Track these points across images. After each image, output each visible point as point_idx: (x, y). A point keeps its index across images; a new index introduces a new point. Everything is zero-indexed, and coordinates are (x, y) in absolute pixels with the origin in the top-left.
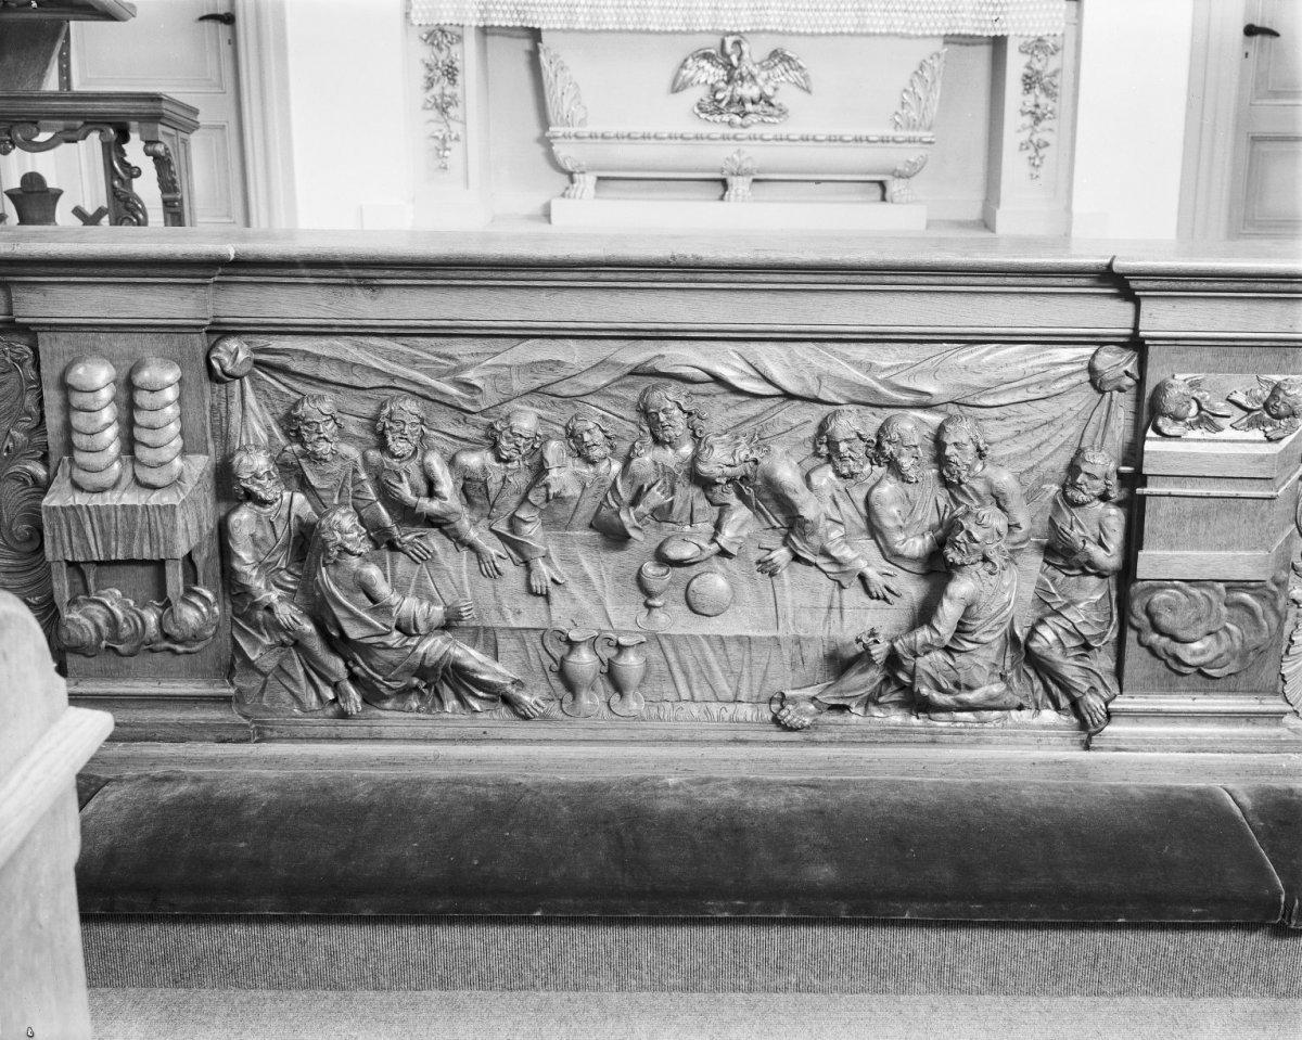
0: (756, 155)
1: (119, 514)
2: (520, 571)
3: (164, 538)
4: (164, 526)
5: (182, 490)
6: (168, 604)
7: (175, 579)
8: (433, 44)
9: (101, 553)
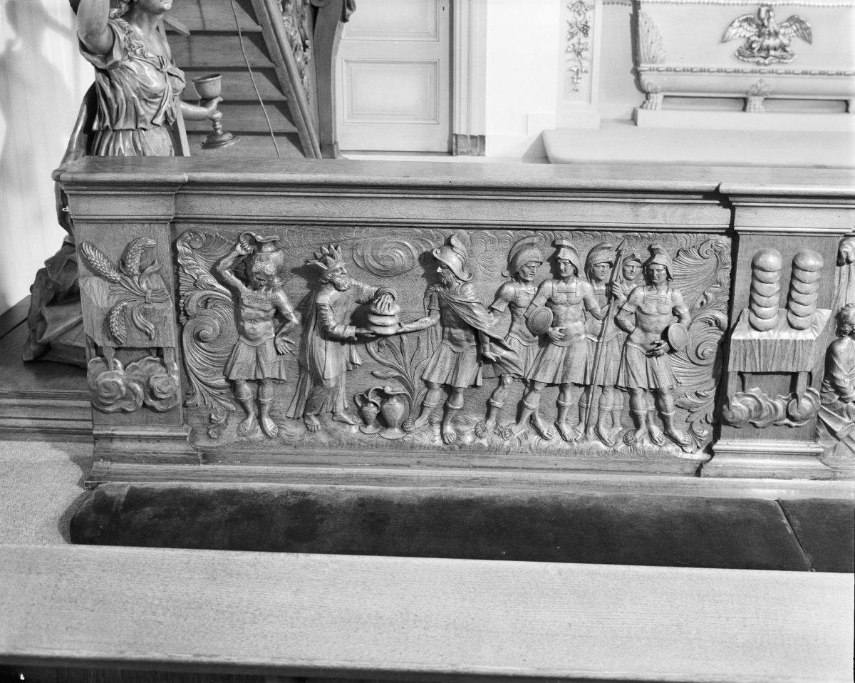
0: (771, 83)
1: (778, 344)
2: (701, 346)
3: (803, 359)
4: (804, 352)
5: (816, 331)
6: (795, 396)
7: (802, 381)
8: (574, 11)
9: (762, 368)
